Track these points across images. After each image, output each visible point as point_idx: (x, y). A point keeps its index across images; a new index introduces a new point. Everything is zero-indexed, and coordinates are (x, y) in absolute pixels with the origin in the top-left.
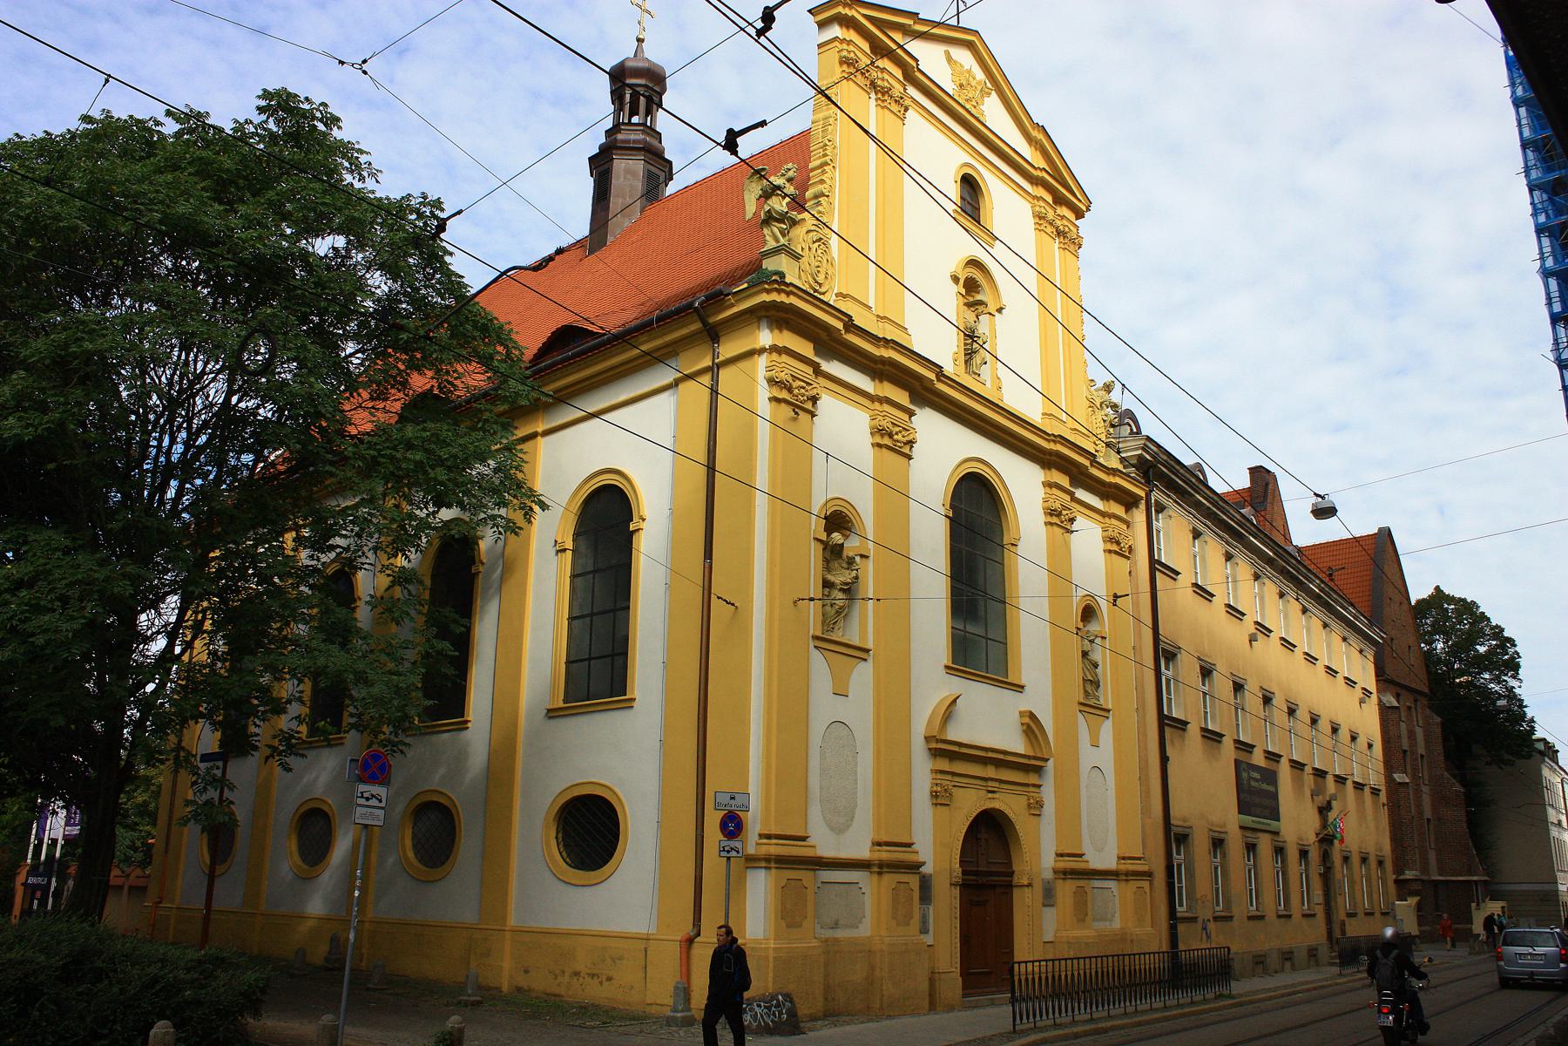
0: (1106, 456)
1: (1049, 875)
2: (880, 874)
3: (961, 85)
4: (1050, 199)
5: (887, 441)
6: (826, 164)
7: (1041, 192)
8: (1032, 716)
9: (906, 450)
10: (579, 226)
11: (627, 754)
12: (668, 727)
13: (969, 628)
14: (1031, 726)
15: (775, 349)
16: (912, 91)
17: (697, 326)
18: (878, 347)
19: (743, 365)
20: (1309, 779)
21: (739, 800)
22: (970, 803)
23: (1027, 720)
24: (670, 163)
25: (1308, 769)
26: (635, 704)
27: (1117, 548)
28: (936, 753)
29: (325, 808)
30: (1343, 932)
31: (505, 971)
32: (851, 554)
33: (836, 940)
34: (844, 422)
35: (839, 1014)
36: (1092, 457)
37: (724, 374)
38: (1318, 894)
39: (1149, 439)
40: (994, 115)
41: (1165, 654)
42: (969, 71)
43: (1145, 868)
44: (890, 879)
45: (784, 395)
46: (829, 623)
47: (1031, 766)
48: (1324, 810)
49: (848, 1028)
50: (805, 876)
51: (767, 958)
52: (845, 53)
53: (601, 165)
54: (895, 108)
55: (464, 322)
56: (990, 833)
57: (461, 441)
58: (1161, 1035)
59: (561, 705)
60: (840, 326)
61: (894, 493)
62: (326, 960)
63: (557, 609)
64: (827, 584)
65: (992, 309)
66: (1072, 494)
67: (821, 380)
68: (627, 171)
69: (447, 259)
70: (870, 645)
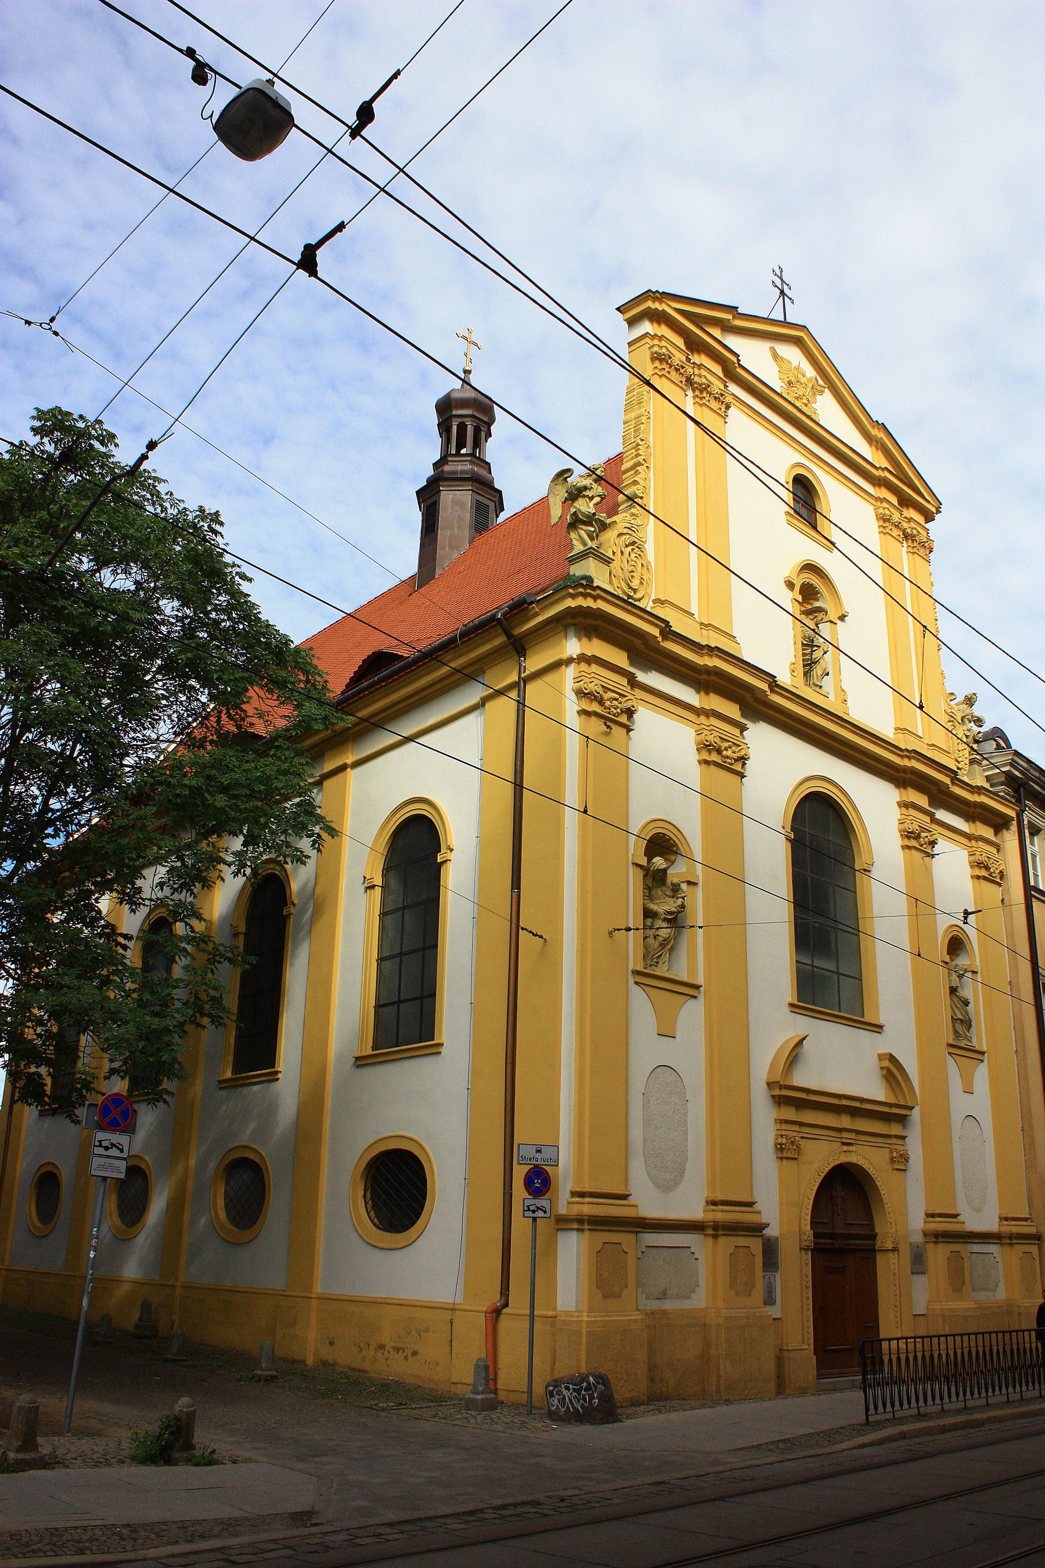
0: (970, 774)
1: (918, 1238)
2: (715, 1236)
3: (790, 383)
5: (715, 757)
6: (639, 464)
7: (884, 493)
8: (892, 1058)
9: (738, 767)
10: (408, 565)
11: (435, 1105)
12: (475, 1072)
13: (817, 963)
14: (892, 1070)
15: (583, 658)
16: (733, 388)
17: (501, 640)
18: (702, 655)
19: (550, 678)
21: (546, 1153)
22: (822, 1156)
23: (886, 1063)
24: (500, 492)
26: (443, 1050)
27: (986, 873)
28: (780, 1101)
29: (143, 1166)
31: (310, 1343)
32: (675, 880)
33: (665, 1313)
34: (665, 739)
35: (666, 1398)
36: (953, 774)
37: (530, 688)
39: (1016, 753)
40: (828, 413)
42: (797, 368)
43: (1033, 1230)
44: (727, 1243)
45: (595, 707)
46: (651, 957)
47: (895, 1115)
49: (673, 1415)
50: (625, 1239)
51: (579, 1332)
52: (656, 349)
53: (428, 497)
54: (715, 405)
55: (271, 658)
56: (846, 1193)
57: (246, 766)
58: (1008, 1440)
59: (370, 1052)
60: (656, 632)
61: (725, 814)
62: (137, 1326)
63: (366, 950)
64: (648, 914)
65: (833, 615)
66: (932, 815)
67: (639, 693)
68: (455, 502)
69: (245, 587)
70: (700, 980)
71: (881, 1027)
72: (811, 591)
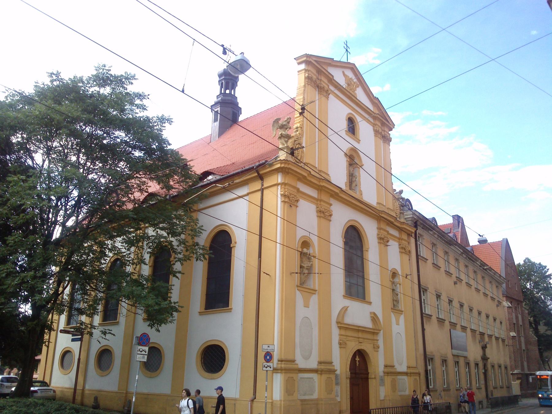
1: (381, 374)
2: (321, 374)
4: (380, 125)
5: (322, 215)
8: (374, 314)
14: (374, 318)
20: (478, 337)
21: (271, 347)
22: (353, 346)
23: (373, 315)
25: (478, 333)
26: (232, 310)
28: (340, 328)
30: (492, 395)
38: (483, 382)
41: (422, 290)
43: (417, 371)
44: (325, 376)
47: (374, 332)
48: (484, 348)
54: (325, 94)
61: (325, 239)
64: (301, 267)
67: (300, 195)
70: (317, 289)
71: (371, 303)
72: (353, 160)
